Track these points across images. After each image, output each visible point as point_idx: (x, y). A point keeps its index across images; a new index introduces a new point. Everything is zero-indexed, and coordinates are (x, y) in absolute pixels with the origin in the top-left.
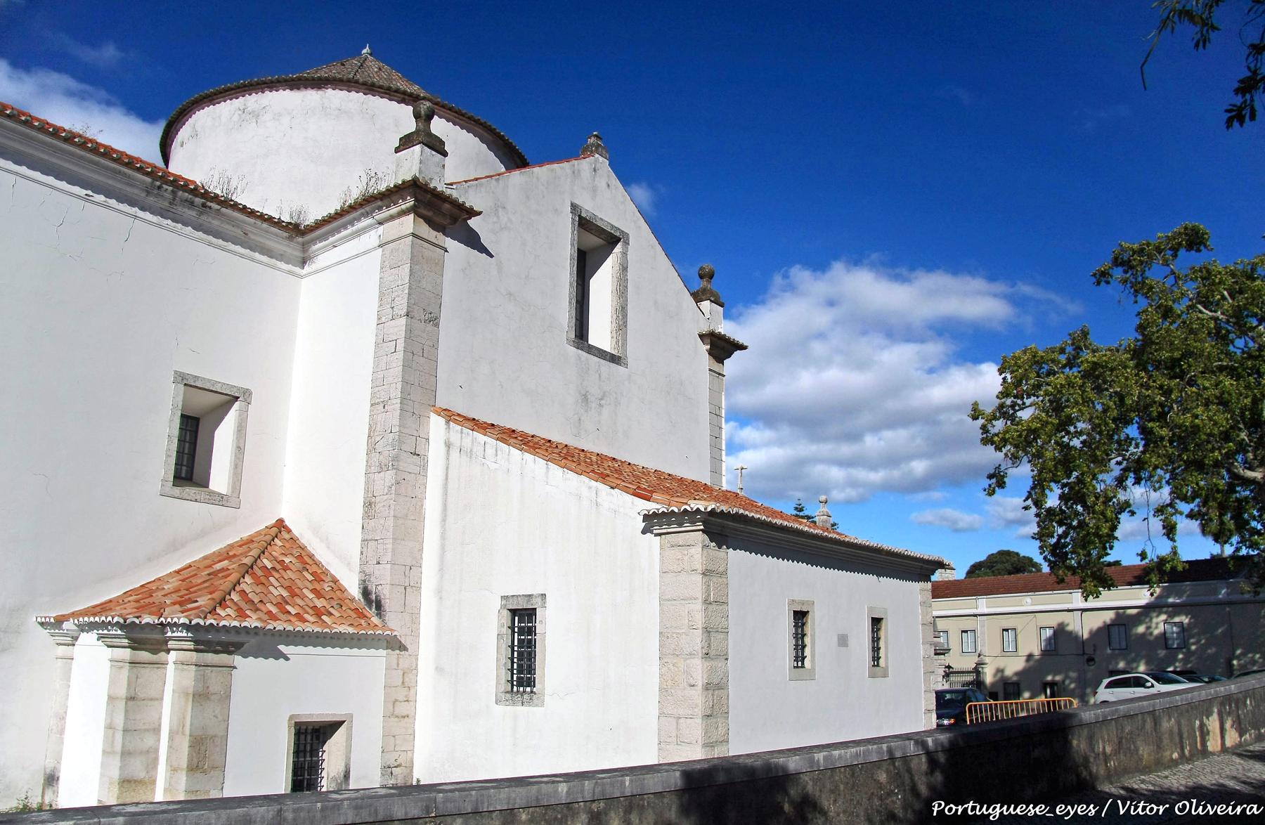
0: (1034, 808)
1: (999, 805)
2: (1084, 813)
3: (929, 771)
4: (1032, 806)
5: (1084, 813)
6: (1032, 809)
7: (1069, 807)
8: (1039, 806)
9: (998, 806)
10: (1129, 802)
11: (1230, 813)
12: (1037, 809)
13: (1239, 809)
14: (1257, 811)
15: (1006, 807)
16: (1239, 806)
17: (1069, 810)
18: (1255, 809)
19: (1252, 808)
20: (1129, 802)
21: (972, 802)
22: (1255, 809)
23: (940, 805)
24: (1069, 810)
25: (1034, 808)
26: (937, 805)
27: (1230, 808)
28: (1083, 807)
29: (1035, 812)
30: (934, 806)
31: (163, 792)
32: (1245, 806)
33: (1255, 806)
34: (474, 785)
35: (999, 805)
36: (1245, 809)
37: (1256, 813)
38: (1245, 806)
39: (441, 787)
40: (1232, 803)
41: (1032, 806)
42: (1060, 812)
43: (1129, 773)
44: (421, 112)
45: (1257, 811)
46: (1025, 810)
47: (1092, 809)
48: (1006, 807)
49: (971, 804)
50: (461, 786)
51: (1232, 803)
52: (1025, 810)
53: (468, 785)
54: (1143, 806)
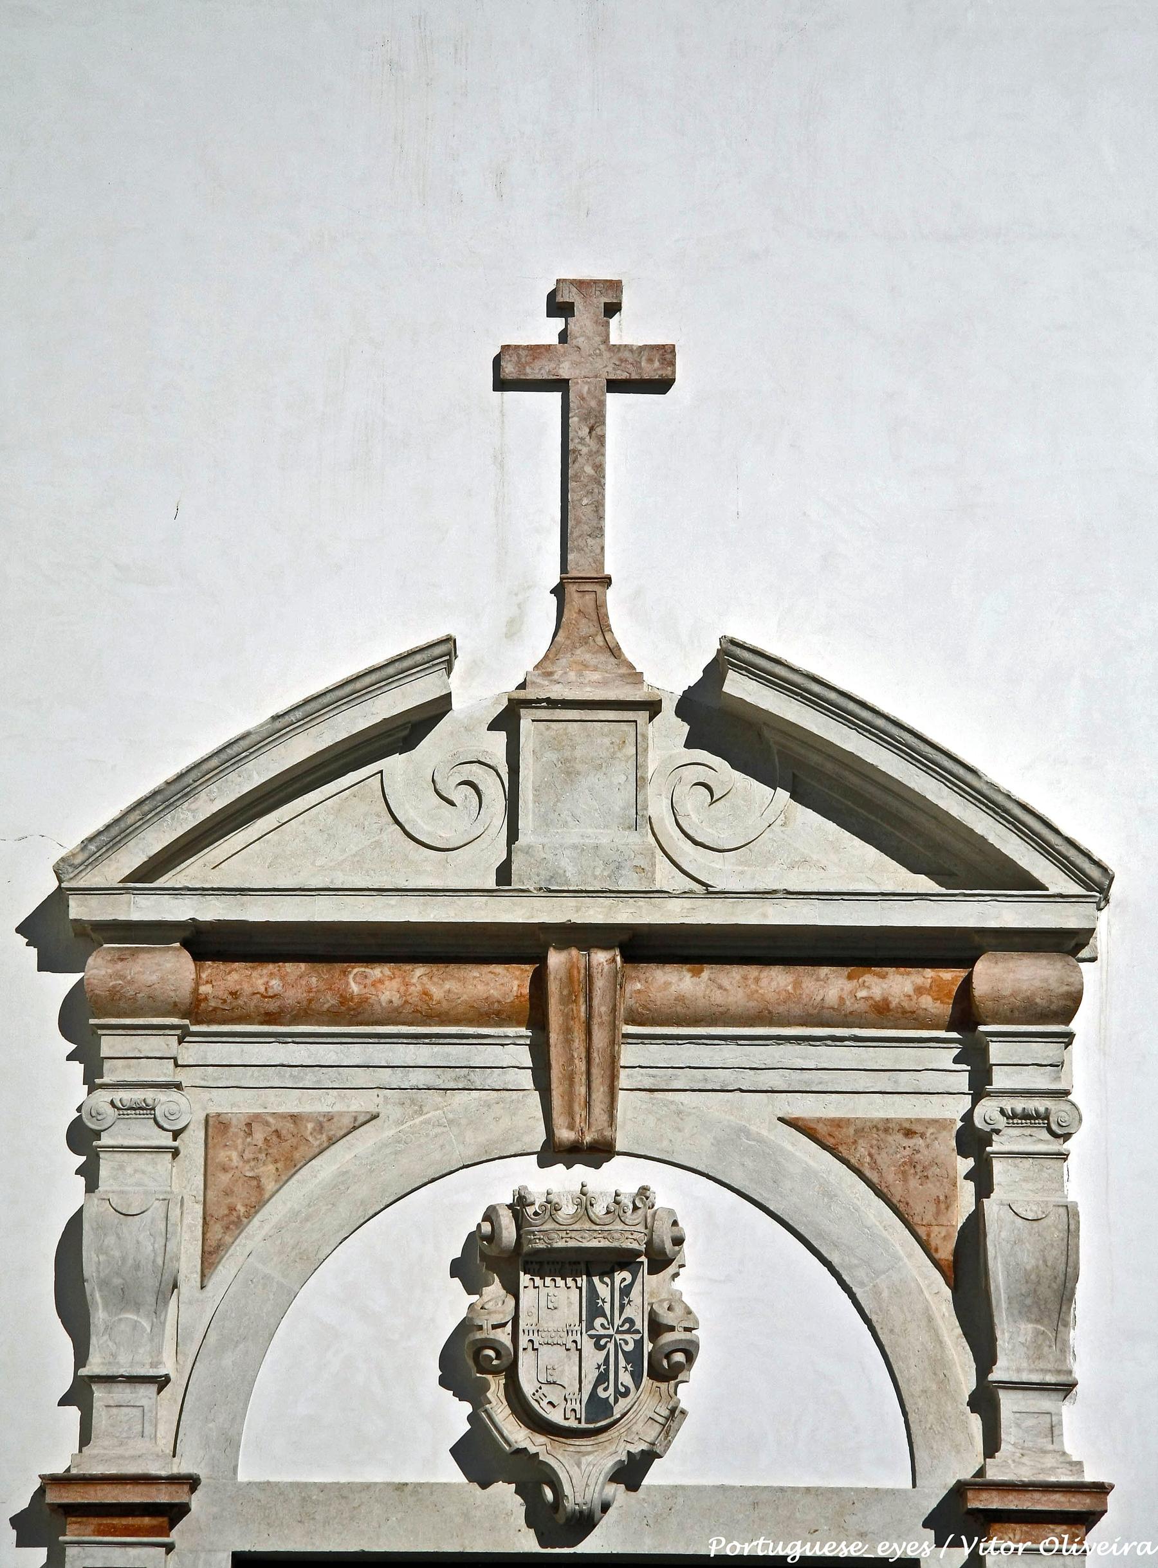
0: (847, 1546)
1: (800, 1542)
2: (1105, 1553)
3: (183, 1008)
4: (844, 1543)
5: (1105, 1553)
6: (844, 1548)
7: (895, 1545)
8: (829, 1543)
9: (799, 1543)
10: (976, 1539)
11: (1115, 1553)
12: (852, 1548)
13: (1126, 1549)
14: (1151, 1550)
15: (809, 1544)
16: (1127, 1544)
17: (895, 1549)
18: (1148, 1549)
19: (1145, 1546)
20: (976, 1539)
21: (763, 1538)
22: (1148, 1549)
23: (719, 1542)
24: (895, 1549)
25: (847, 1546)
26: (715, 1543)
27: (1115, 1546)
28: (1104, 1545)
29: (849, 1551)
30: (711, 1544)
31: (623, 305)
32: (1135, 1543)
33: (1149, 1544)
34: (880, 722)
35: (800, 1542)
36: (1135, 1548)
37: (1150, 1553)
38: (1135, 1543)
39: (507, 790)
40: (1117, 1540)
41: (844, 1543)
42: (1102, 1551)
43: (928, 1310)
44: (65, 1535)
45: (1151, 1550)
46: (918, 1549)
47: (926, 1548)
48: (809, 1544)
49: (761, 1541)
50: (778, 670)
51: (1117, 1540)
52: (918, 1549)
53: (865, 714)
54: (763, 1544)
